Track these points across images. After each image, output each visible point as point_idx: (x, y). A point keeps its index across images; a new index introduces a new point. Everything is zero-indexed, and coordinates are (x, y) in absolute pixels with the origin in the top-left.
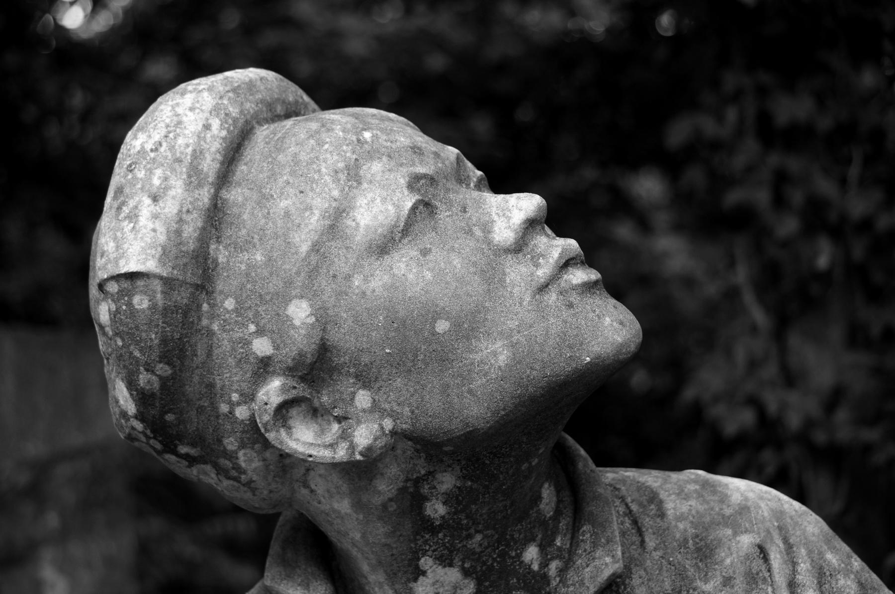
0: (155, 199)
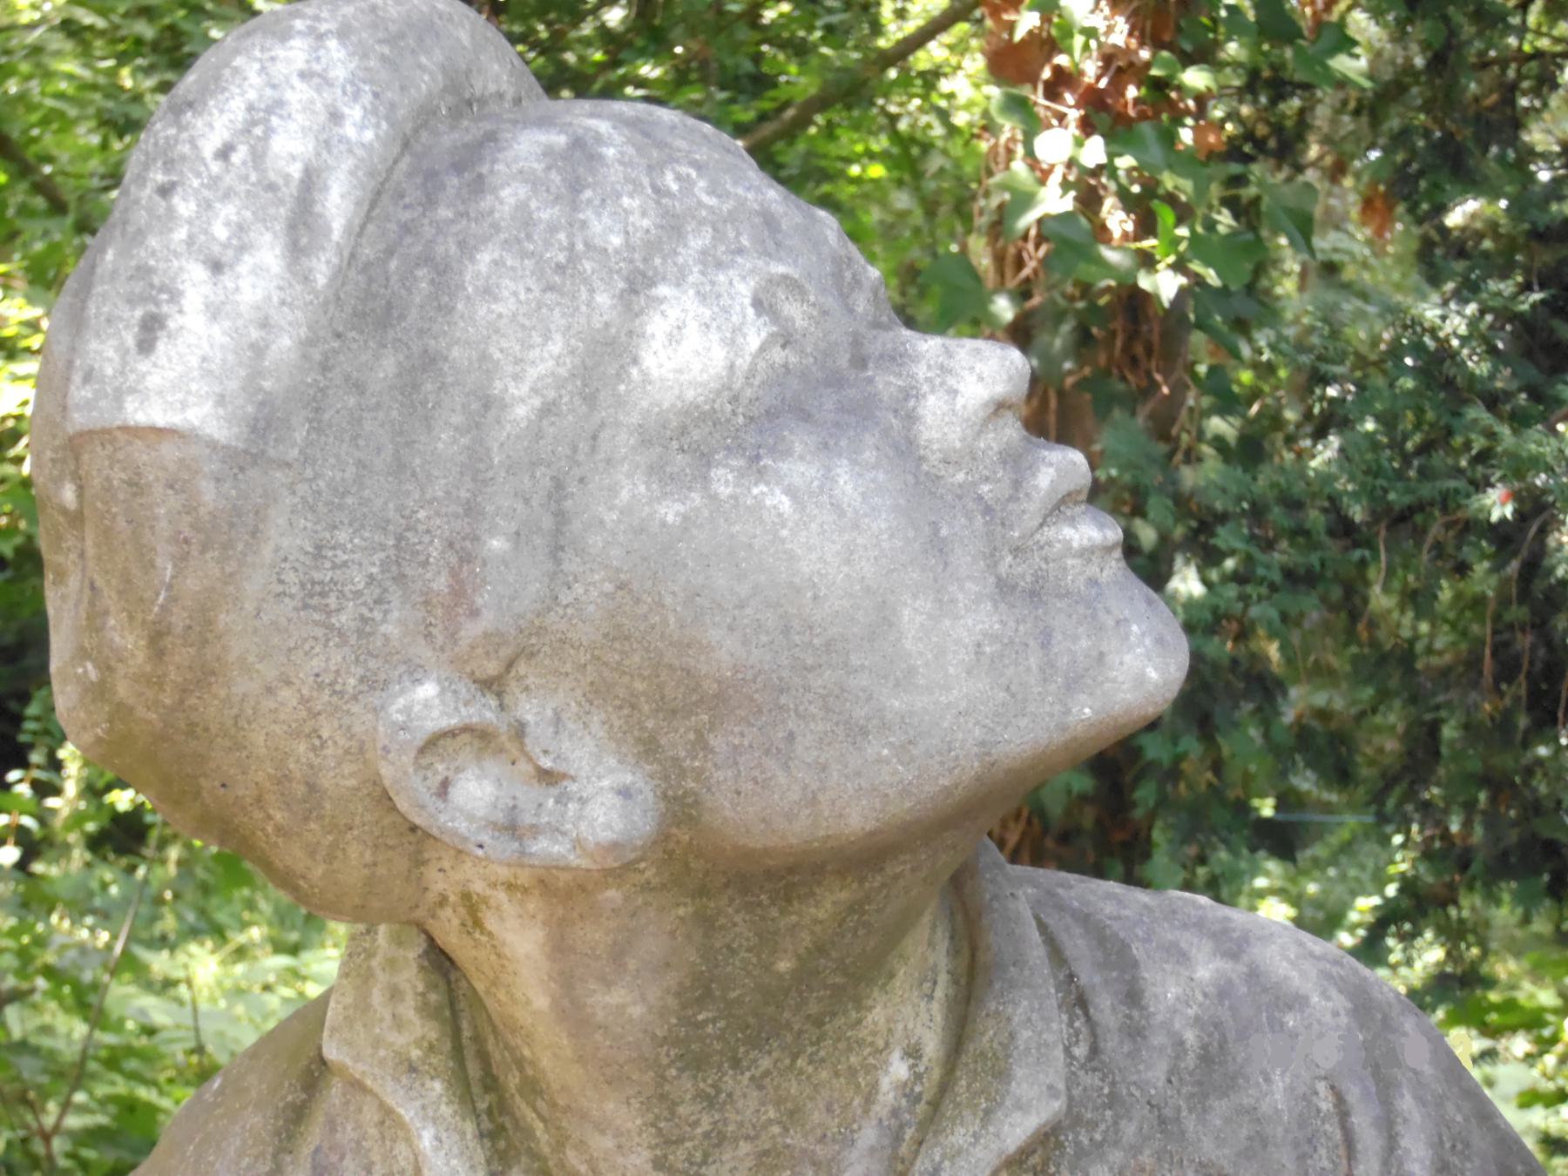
0: (216, 267)
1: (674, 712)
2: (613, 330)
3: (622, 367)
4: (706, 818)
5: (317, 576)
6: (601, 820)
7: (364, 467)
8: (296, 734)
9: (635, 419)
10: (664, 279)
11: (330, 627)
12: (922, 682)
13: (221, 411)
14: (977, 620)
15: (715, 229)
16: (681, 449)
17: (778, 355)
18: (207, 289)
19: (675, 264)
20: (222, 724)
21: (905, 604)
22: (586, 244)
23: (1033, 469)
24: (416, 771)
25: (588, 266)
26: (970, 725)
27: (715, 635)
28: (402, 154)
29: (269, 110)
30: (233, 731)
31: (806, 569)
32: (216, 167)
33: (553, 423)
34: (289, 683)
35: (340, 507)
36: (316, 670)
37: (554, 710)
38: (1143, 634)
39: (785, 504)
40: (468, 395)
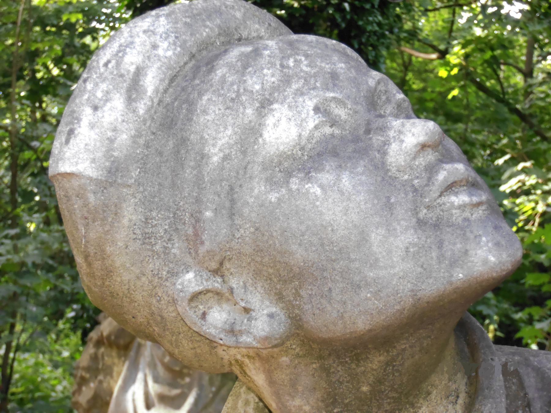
0: (96, 108)
1: (286, 281)
2: (253, 124)
3: (256, 138)
4: (305, 325)
5: (147, 231)
6: (260, 327)
7: (161, 185)
8: (151, 296)
9: (261, 160)
10: (277, 101)
11: (153, 251)
12: (382, 264)
13: (93, 165)
14: (406, 237)
15: (305, 80)
16: (280, 171)
17: (328, 130)
18: (91, 117)
19: (283, 95)
20: (123, 292)
21: (372, 231)
22: (244, 89)
23: (437, 172)
24: (190, 309)
25: (244, 98)
26: (406, 283)
27: (294, 247)
28: (190, 60)
29: (127, 46)
30: (129, 295)
31: (327, 218)
32: (102, 70)
33: (229, 163)
34: (144, 275)
35: (153, 202)
36: (151, 269)
37: (243, 282)
38: (488, 242)
39: (318, 191)
40: (196, 153)
